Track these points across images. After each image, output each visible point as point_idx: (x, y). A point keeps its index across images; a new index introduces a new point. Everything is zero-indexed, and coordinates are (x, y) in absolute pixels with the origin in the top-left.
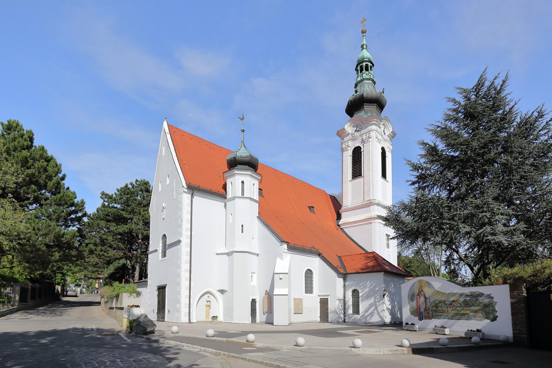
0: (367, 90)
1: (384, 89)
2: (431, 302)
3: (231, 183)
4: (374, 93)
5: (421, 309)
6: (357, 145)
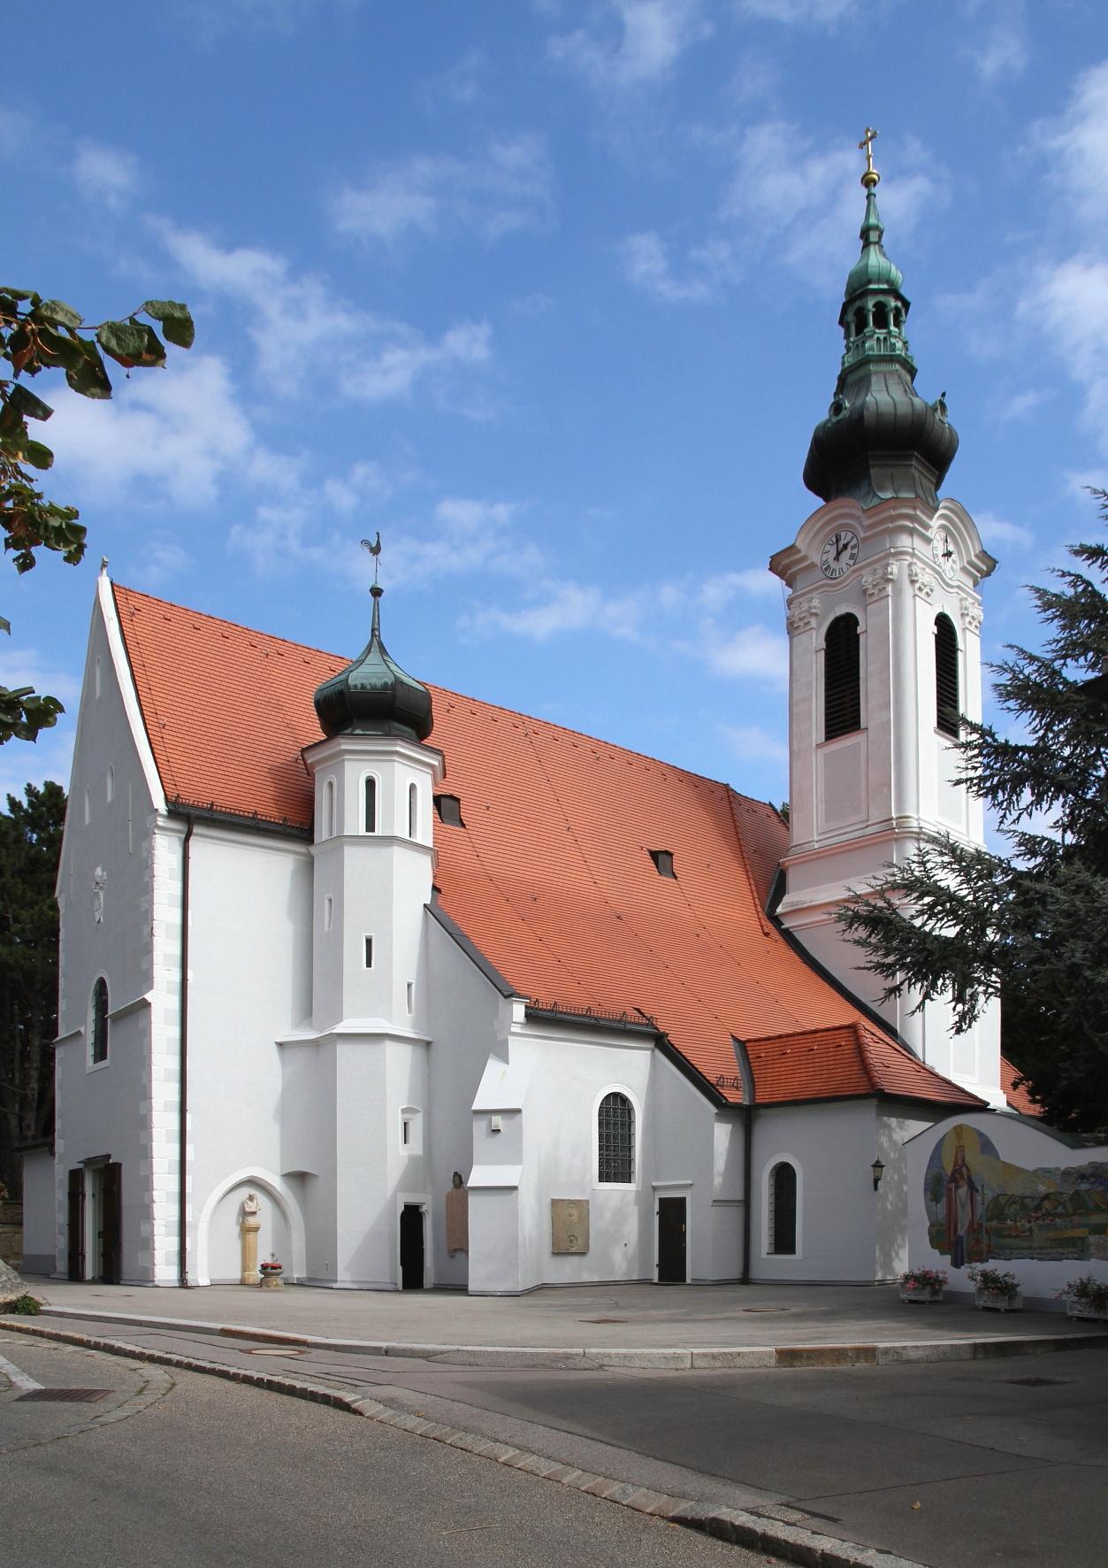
0: (883, 396)
1: (944, 395)
2: (986, 1203)
3: (331, 785)
4: (903, 409)
5: (959, 1227)
6: (841, 610)
